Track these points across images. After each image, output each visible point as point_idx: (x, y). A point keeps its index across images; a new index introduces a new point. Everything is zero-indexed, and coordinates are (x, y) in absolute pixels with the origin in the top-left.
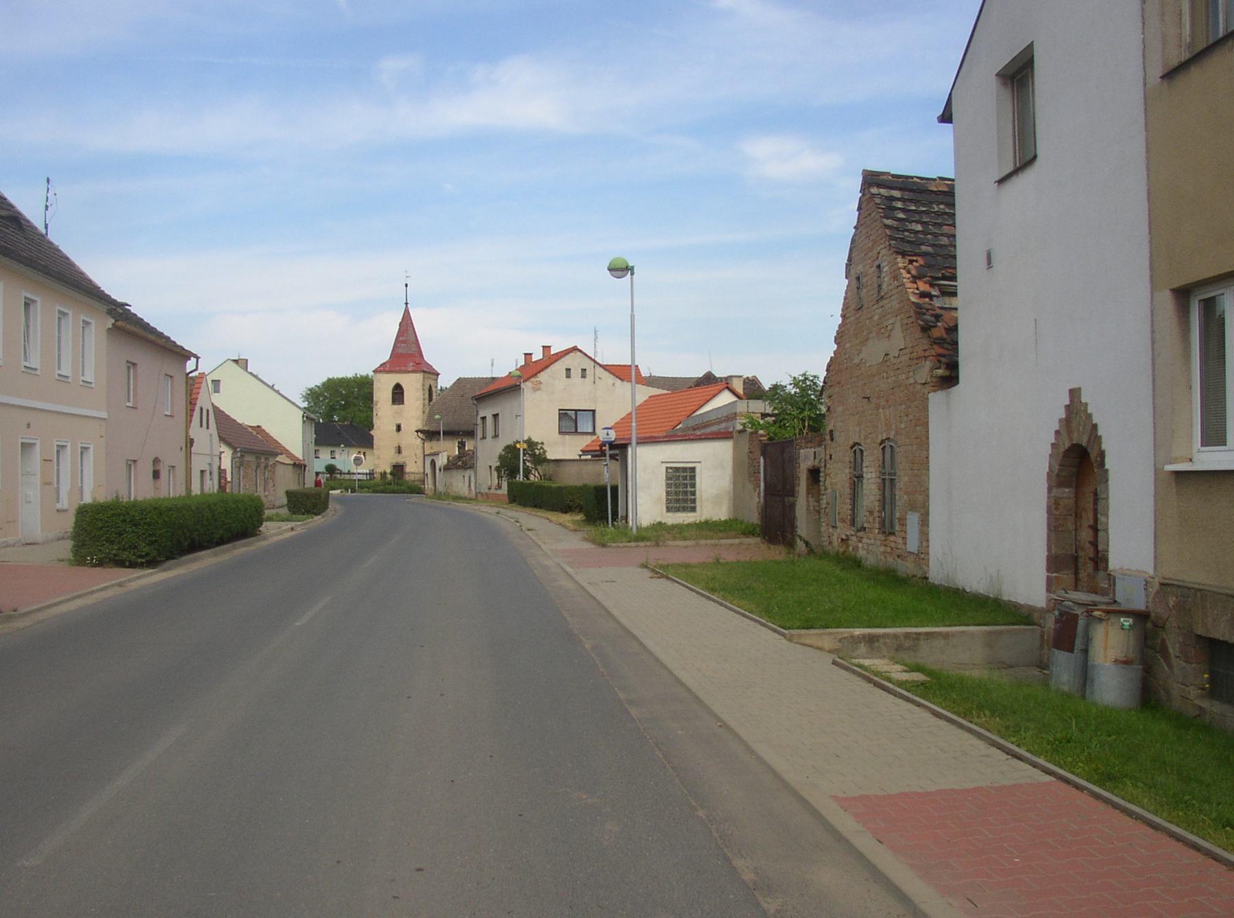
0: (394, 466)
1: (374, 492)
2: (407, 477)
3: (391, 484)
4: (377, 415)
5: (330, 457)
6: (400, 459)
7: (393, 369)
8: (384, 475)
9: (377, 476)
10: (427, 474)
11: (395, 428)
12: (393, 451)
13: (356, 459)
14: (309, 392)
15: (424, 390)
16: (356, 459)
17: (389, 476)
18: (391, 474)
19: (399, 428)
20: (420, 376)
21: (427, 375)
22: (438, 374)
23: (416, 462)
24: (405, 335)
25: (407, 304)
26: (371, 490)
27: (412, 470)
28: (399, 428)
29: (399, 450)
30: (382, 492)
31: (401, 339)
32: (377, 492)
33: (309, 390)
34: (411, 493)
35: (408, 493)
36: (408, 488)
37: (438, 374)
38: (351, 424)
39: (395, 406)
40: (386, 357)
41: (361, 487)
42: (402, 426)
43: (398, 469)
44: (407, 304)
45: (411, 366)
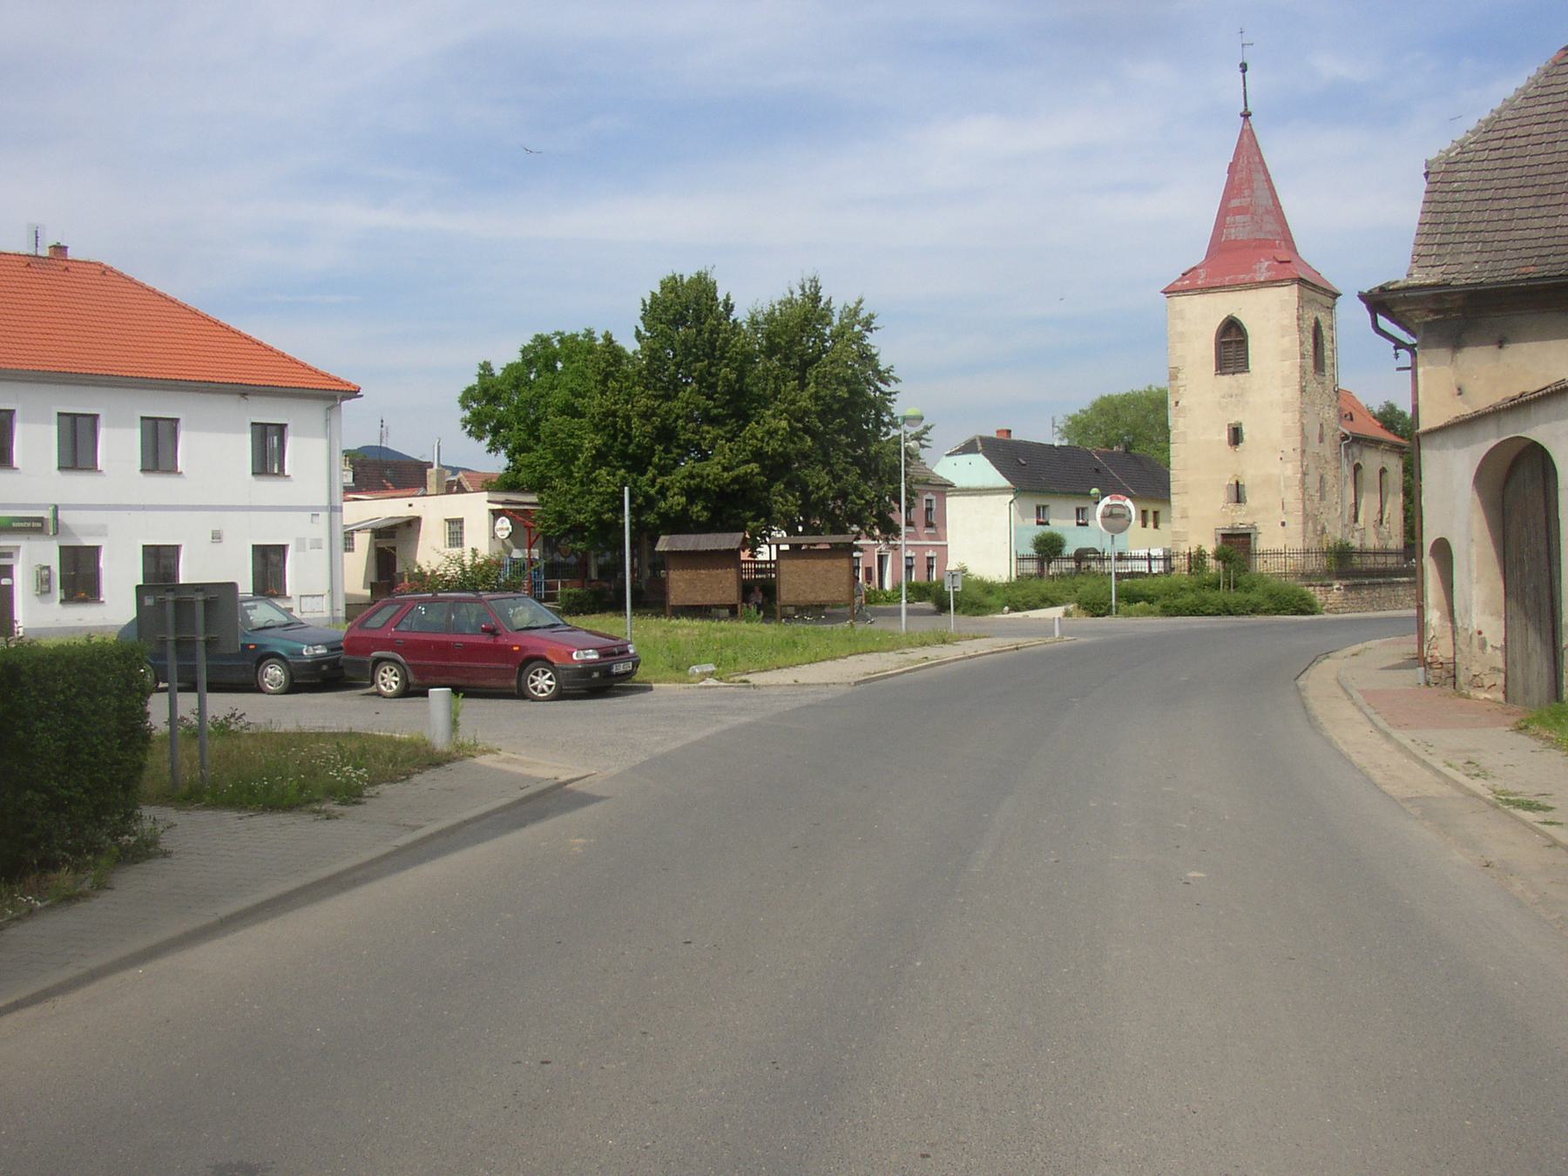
0: (1224, 535)
1: (1167, 611)
2: (1260, 566)
3: (1217, 586)
4: (1177, 403)
5: (1035, 521)
6: (1239, 518)
7: (1217, 281)
8: (1197, 559)
9: (1180, 563)
10: (1443, 550)
11: (1225, 436)
12: (1222, 496)
13: (1111, 515)
14: (1070, 423)
15: (1301, 330)
16: (1111, 515)
17: (1212, 564)
18: (1217, 557)
19: (1236, 436)
20: (1290, 294)
21: (1308, 293)
22: (1336, 295)
23: (1283, 524)
24: (1246, 192)
25: (1246, 115)
26: (1156, 607)
27: (1278, 545)
28: (1236, 436)
29: (1238, 494)
30: (1194, 613)
31: (1235, 203)
32: (1179, 612)
33: (1070, 419)
34: (1278, 612)
35: (1266, 612)
36: (1271, 596)
37: (1336, 295)
38: (1127, 451)
39: (1227, 379)
40: (1198, 256)
41: (1130, 597)
42: (1245, 430)
43: (1236, 544)
44: (1246, 115)
45: (1263, 270)
